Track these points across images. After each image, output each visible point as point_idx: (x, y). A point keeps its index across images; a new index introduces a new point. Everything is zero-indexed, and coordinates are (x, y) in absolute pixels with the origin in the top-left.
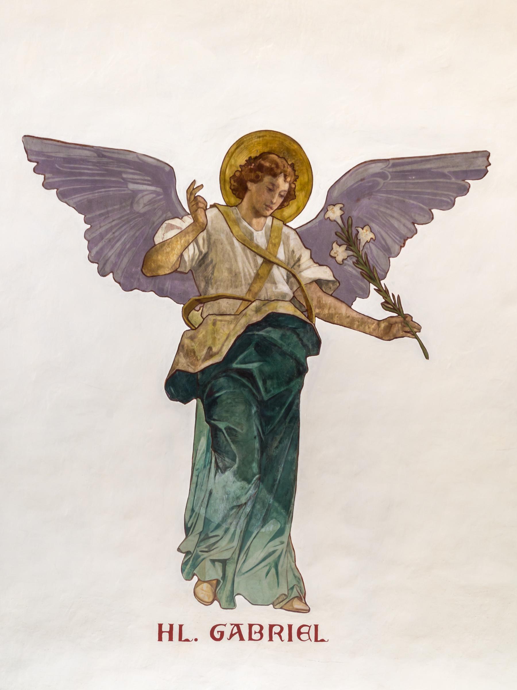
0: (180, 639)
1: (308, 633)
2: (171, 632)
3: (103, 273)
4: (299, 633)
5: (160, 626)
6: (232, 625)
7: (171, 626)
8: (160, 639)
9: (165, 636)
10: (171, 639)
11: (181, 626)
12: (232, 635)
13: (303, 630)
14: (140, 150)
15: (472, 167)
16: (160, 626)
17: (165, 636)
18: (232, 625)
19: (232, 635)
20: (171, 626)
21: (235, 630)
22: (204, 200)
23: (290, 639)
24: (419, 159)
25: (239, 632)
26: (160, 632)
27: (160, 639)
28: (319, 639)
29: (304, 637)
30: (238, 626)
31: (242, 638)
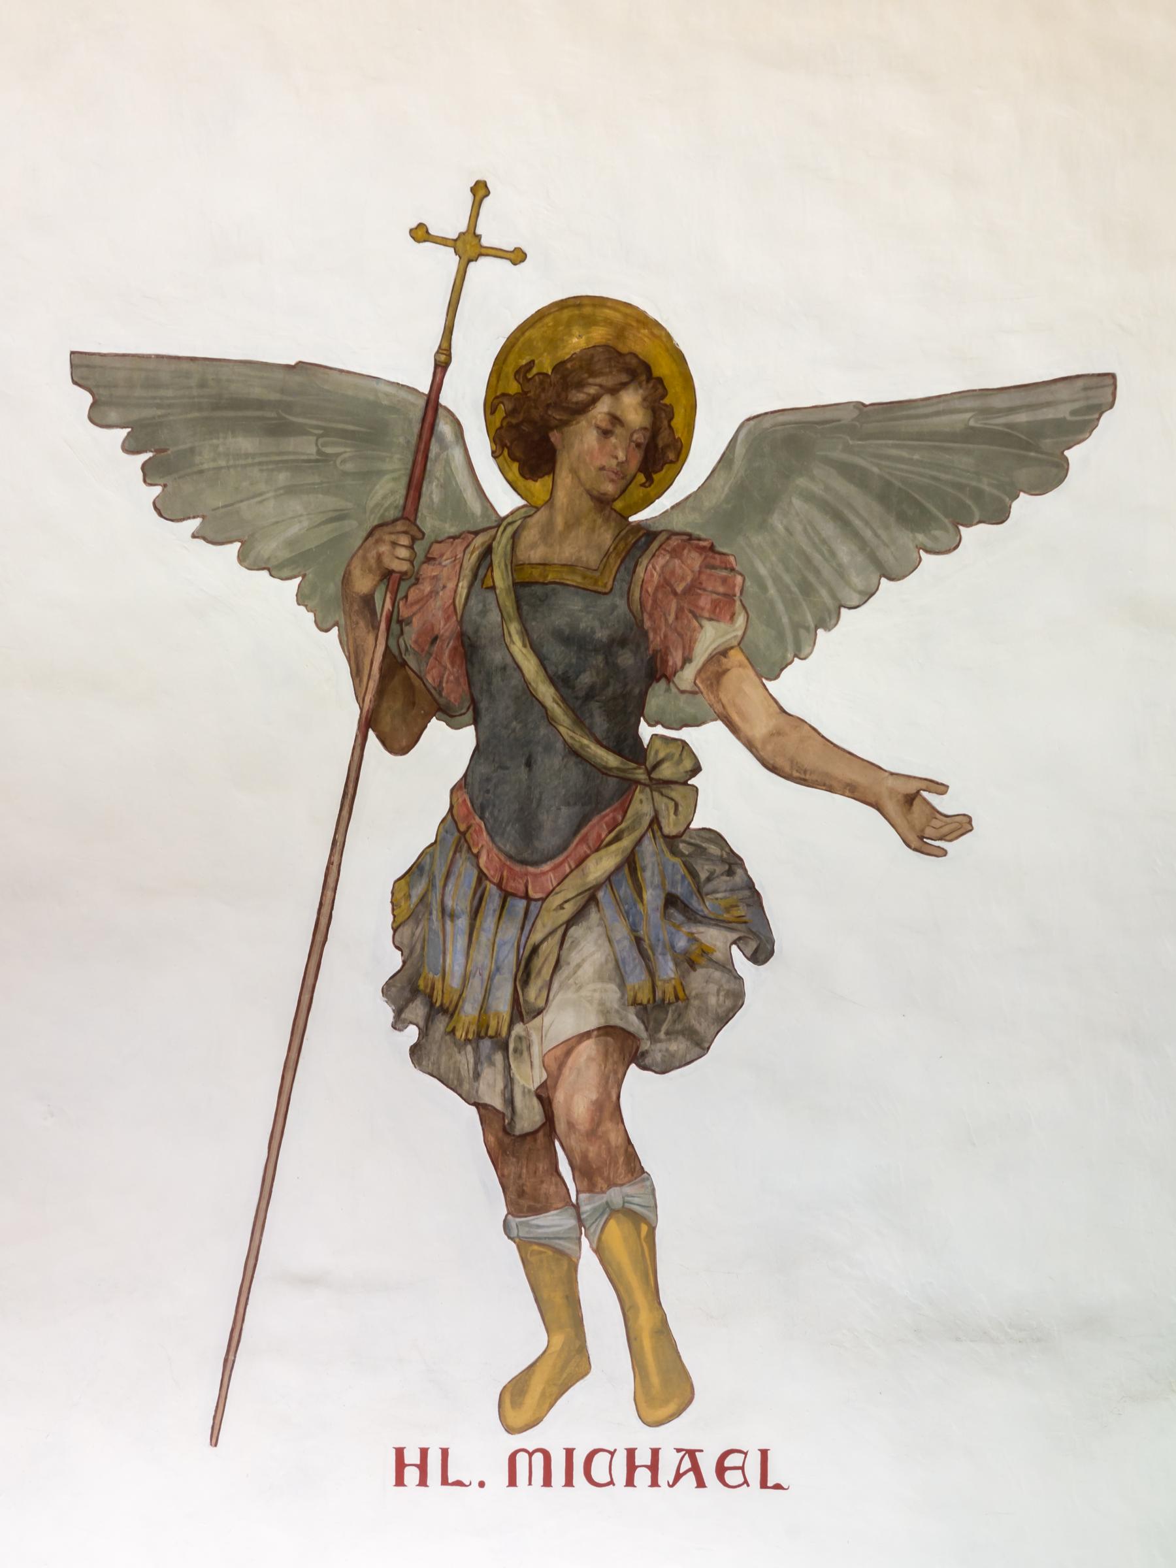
0: (445, 1481)
1: (742, 1468)
2: (423, 1467)
3: (999, 515)
4: (721, 1470)
5: (400, 1452)
6: (679, 1450)
7: (424, 1452)
8: (400, 1481)
9: (411, 1475)
10: (423, 1482)
11: (445, 1453)
12: (678, 1476)
13: (733, 1460)
14: (529, 315)
15: (1088, 399)
16: (400, 1452)
17: (411, 1475)
18: (679, 1450)
19: (678, 1476)
20: (424, 1452)
21: (687, 1464)
22: (749, 420)
23: (569, 1482)
24: (412, 493)
25: (696, 1468)
26: (400, 1465)
27: (400, 1481)
28: (770, 1484)
29: (733, 1477)
30: (692, 1454)
31: (701, 1483)
